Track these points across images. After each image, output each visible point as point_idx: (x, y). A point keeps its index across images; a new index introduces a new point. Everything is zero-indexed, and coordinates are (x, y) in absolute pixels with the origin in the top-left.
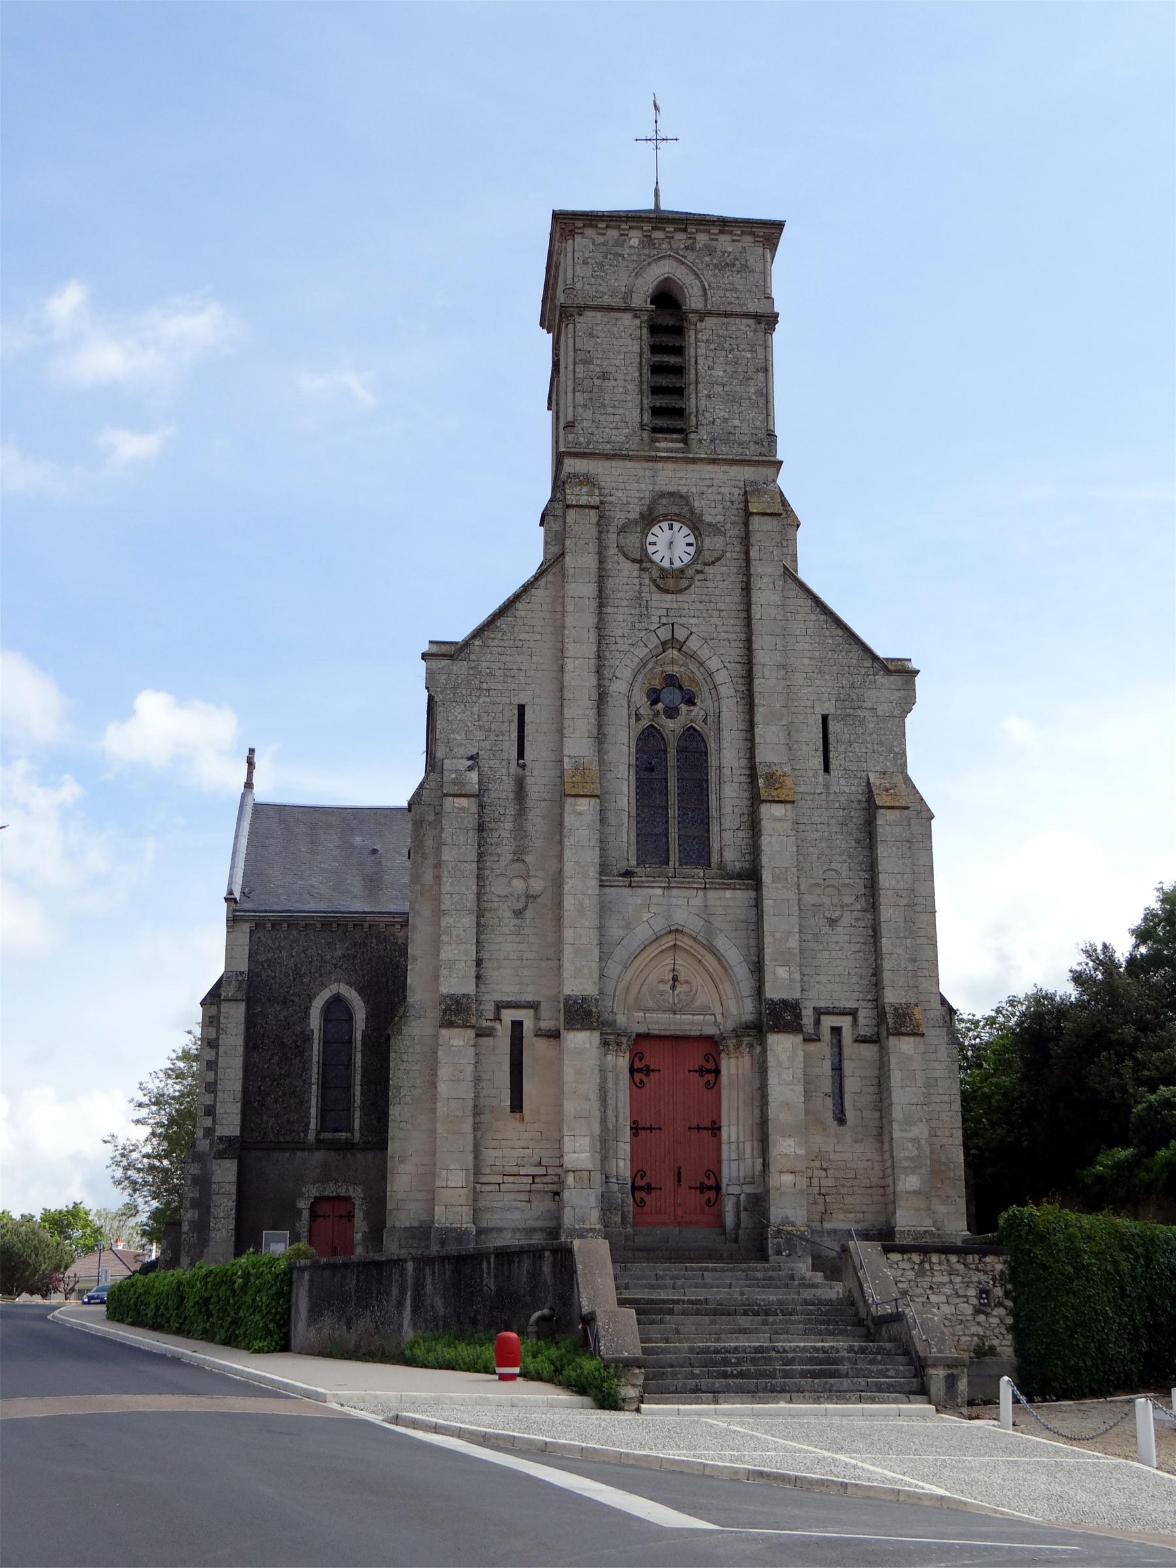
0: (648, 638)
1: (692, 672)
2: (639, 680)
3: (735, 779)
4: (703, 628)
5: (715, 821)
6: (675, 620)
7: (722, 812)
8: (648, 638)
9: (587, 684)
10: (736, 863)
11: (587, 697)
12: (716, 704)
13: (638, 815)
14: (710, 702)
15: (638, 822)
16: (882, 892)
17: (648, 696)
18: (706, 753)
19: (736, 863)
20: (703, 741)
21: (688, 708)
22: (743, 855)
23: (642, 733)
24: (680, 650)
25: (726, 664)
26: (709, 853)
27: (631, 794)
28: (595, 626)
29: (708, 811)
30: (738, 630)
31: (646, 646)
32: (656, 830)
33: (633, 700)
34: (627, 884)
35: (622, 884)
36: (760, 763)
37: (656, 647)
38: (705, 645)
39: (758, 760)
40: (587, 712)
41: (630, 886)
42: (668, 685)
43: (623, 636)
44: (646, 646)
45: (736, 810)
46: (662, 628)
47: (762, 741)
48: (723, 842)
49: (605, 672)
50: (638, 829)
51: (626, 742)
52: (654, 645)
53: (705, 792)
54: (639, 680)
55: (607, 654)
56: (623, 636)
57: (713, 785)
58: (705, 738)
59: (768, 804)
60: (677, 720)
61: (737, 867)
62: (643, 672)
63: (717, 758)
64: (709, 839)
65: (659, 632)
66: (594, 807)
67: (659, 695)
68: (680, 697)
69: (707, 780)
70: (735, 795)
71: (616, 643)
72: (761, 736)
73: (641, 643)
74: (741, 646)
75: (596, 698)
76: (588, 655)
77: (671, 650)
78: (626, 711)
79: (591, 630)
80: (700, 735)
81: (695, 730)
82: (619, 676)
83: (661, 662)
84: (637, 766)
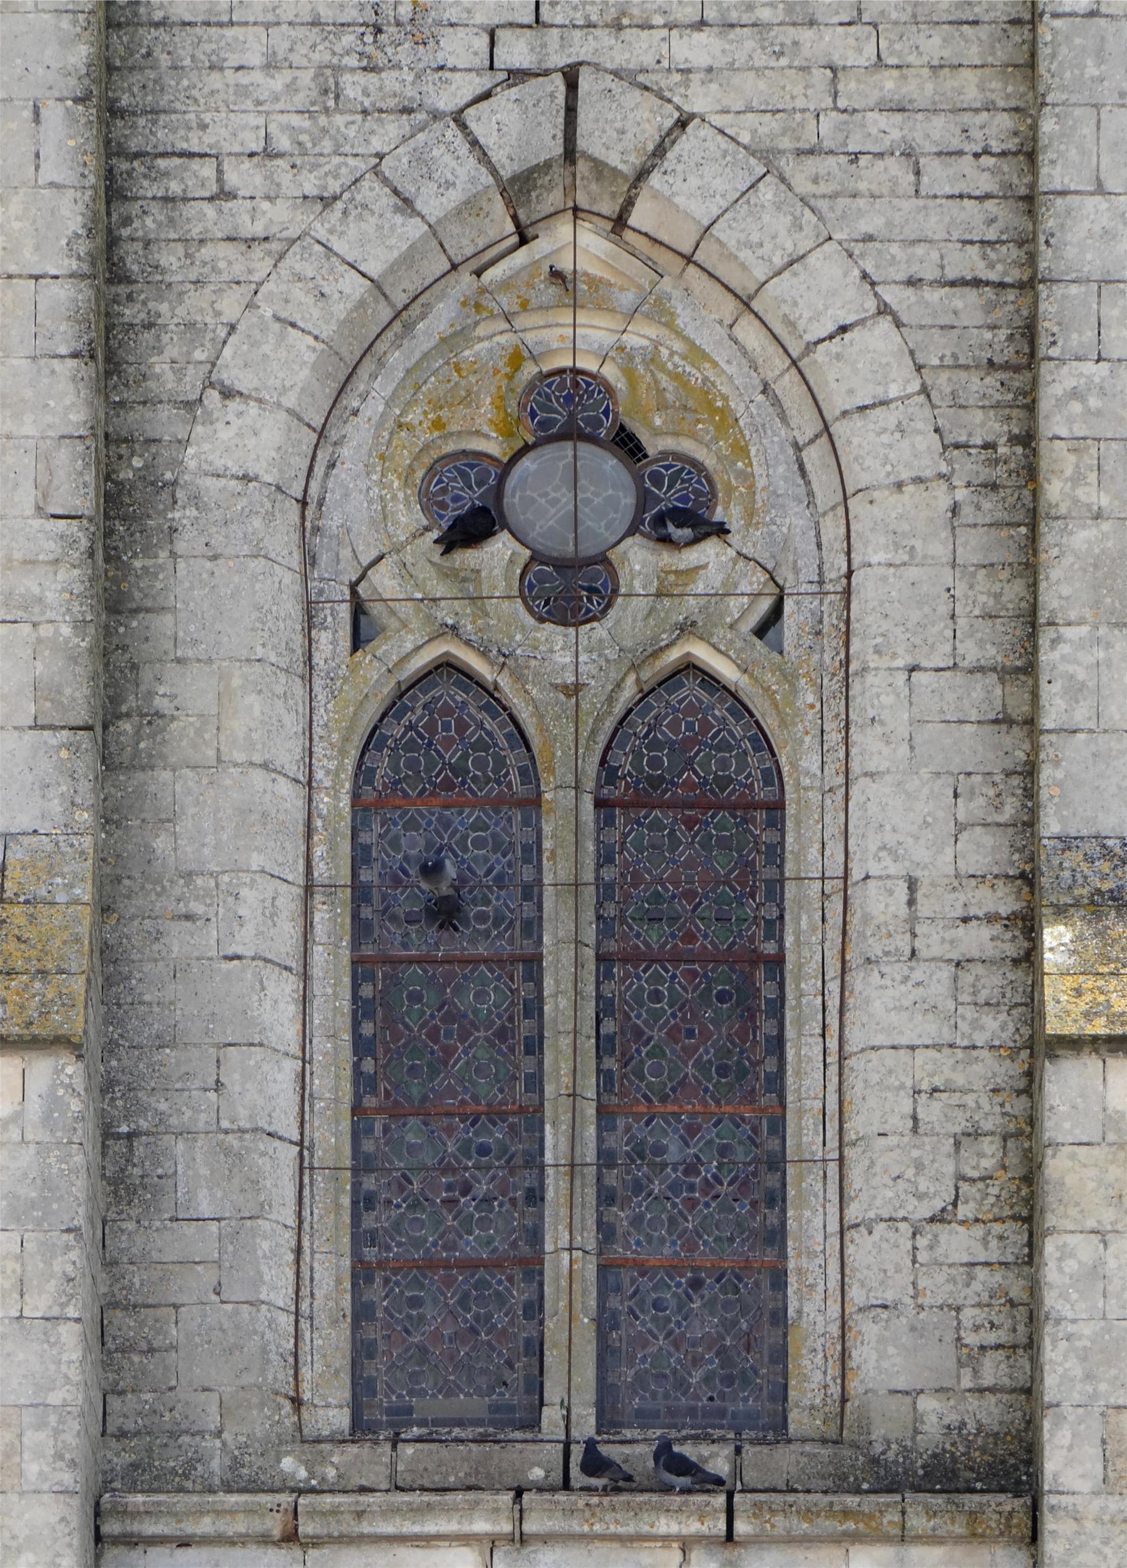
0: (420, 159)
1: (696, 354)
2: (374, 408)
3: (932, 941)
4: (754, 88)
5: (812, 1181)
6: (581, 48)
7: (855, 1126)
8: (420, 159)
9: (29, 429)
10: (927, 1404)
11: (27, 498)
12: (833, 530)
13: (362, 1164)
14: (796, 519)
15: (363, 1202)
16: (1047, 1368)
17: (430, 502)
18: (776, 808)
19: (927, 1404)
20: (762, 742)
21: (667, 558)
22: (971, 1358)
23: (394, 708)
24: (620, 223)
25: (889, 295)
26: (780, 1356)
27: (321, 1046)
28: (74, 87)
29: (778, 1126)
30: (972, 95)
31: (406, 204)
32: (471, 1245)
33: (333, 522)
34: (275, 1526)
35: (240, 1526)
36: (1067, 842)
37: (470, 207)
38: (767, 192)
39: (1051, 825)
40: (30, 584)
41: (291, 1537)
42: (549, 434)
43: (269, 153)
44: (406, 204)
45: (931, 1111)
46: (505, 99)
47: (1081, 715)
48: (856, 1295)
49: (160, 366)
50: (360, 1238)
51: (288, 754)
52: (455, 197)
53: (767, 1027)
54: (374, 408)
55: (170, 258)
56: (269, 153)
57: (810, 985)
58: (770, 723)
59: (1089, 1065)
60: (599, 630)
61: (932, 1427)
62: (398, 360)
63: (833, 827)
64: (779, 1280)
65: (481, 121)
66: (52, 1103)
67: (498, 491)
68: (628, 501)
69: (779, 960)
70: (929, 1029)
71: (224, 194)
72: (1075, 690)
73: (372, 191)
74: (986, 183)
75: (85, 502)
76: (30, 260)
77: (564, 229)
78: (290, 581)
79: (54, 113)
80: (740, 707)
81: (710, 681)
82: (243, 381)
83: (507, 301)
84: (360, 894)
